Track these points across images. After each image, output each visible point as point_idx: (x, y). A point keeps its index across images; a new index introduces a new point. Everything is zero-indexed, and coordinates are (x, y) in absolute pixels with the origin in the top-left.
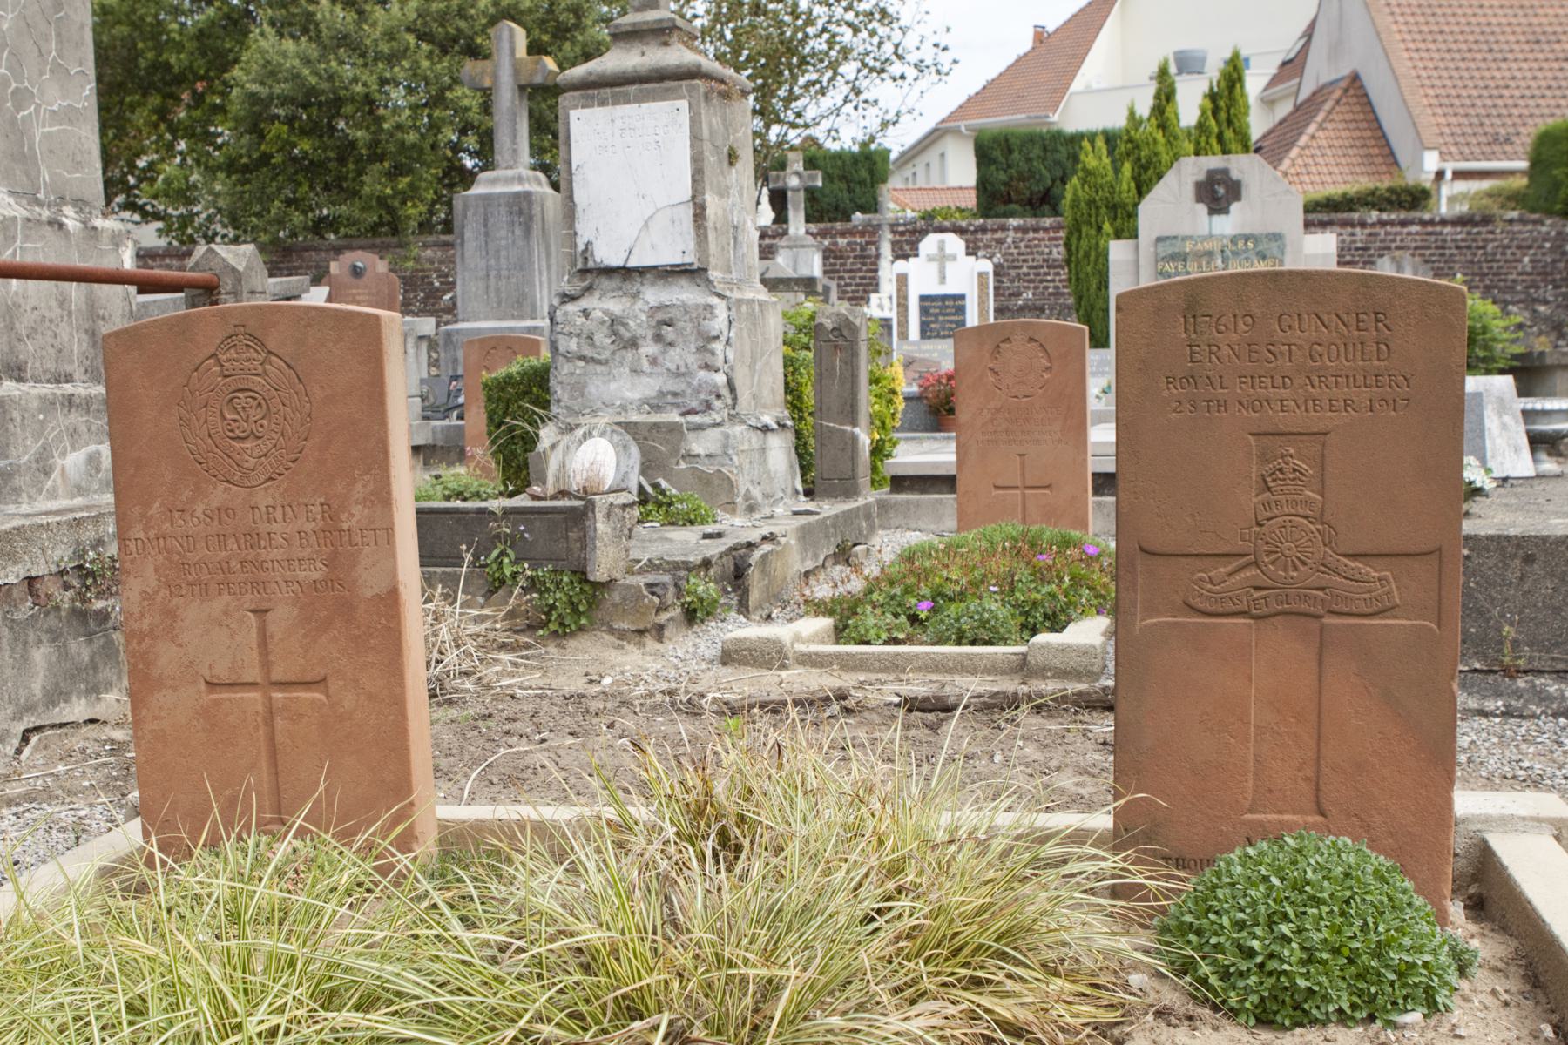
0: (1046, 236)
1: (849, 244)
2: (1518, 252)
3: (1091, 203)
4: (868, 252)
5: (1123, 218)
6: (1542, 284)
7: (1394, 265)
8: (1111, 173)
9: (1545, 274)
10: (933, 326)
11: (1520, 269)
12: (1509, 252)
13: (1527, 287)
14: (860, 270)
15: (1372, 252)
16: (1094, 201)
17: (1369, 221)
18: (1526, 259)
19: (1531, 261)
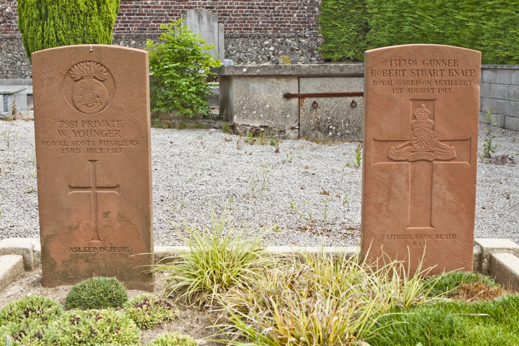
7: (197, 14)
9: (306, 23)
15: (215, 9)
18: (295, 15)
19: (297, 16)
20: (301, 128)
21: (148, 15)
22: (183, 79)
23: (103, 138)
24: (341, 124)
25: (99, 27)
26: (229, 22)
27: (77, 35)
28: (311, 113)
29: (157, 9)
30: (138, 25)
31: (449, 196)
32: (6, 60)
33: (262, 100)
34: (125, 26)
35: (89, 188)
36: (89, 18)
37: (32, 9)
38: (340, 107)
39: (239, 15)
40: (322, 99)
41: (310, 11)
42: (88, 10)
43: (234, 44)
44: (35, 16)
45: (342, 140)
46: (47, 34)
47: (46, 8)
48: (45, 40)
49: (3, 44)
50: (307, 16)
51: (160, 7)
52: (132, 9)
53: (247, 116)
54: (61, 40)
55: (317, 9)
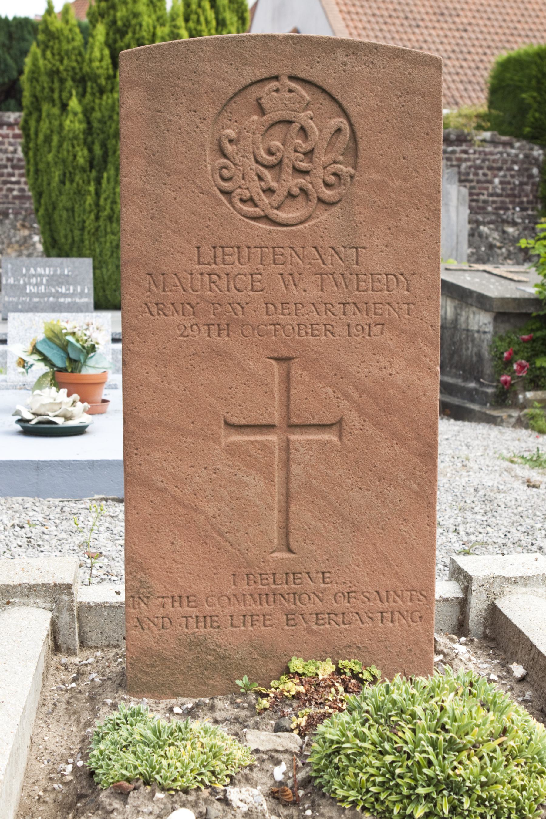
0: (10, 132)
2: (489, 173)
3: (53, 73)
5: (93, 94)
6: (511, 206)
8: (79, 38)
9: (514, 196)
11: (490, 190)
12: (481, 172)
13: (496, 209)
16: (58, 72)
18: (497, 181)
19: (501, 183)
37: (73, 147)
41: (523, 175)
44: (81, 161)
46: (109, 201)
48: (105, 214)
50: (517, 182)
55: (535, 171)
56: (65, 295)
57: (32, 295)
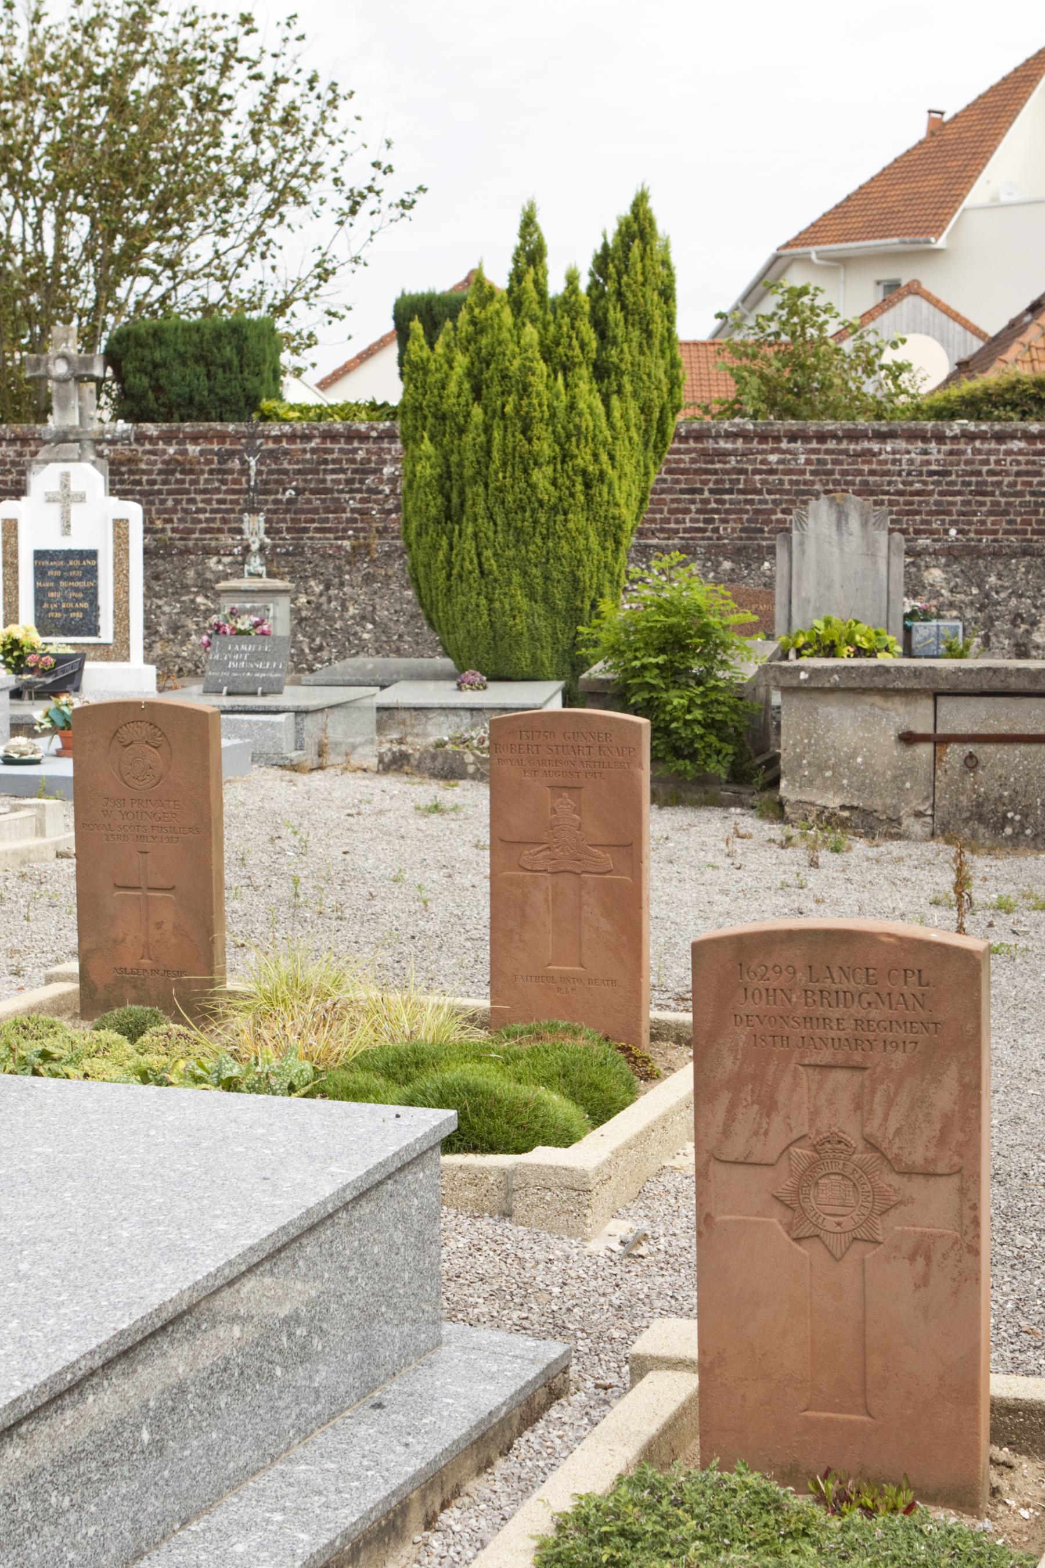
1: (202, 453)
4: (230, 465)
5: (452, 434)
7: (833, 510)
10: (52, 595)
14: (218, 490)
15: (953, 477)
17: (949, 433)
20: (939, 814)
21: (769, 492)
22: (673, 693)
23: (156, 823)
24: (1036, 808)
25: (587, 539)
26: (990, 513)
27: (529, 561)
28: (962, 780)
29: (794, 478)
30: (741, 519)
31: (605, 924)
32: (398, 608)
33: (848, 745)
34: (707, 521)
35: (138, 888)
36: (560, 518)
38: (1034, 768)
39: (1020, 494)
40: (990, 749)
42: (560, 499)
43: (1005, 573)
44: (433, 511)
45: (1036, 848)
47: (462, 493)
48: (455, 572)
49: (392, 566)
51: (802, 472)
52: (726, 477)
53: (810, 782)
54: (491, 573)
56: (261, 671)
57: (232, 670)
